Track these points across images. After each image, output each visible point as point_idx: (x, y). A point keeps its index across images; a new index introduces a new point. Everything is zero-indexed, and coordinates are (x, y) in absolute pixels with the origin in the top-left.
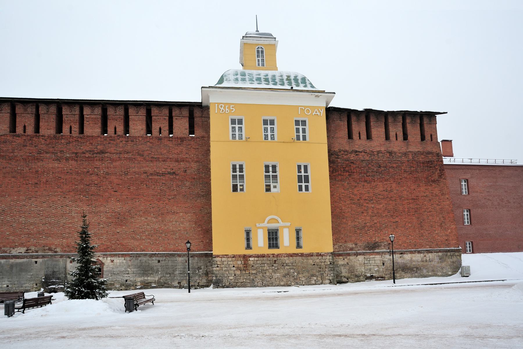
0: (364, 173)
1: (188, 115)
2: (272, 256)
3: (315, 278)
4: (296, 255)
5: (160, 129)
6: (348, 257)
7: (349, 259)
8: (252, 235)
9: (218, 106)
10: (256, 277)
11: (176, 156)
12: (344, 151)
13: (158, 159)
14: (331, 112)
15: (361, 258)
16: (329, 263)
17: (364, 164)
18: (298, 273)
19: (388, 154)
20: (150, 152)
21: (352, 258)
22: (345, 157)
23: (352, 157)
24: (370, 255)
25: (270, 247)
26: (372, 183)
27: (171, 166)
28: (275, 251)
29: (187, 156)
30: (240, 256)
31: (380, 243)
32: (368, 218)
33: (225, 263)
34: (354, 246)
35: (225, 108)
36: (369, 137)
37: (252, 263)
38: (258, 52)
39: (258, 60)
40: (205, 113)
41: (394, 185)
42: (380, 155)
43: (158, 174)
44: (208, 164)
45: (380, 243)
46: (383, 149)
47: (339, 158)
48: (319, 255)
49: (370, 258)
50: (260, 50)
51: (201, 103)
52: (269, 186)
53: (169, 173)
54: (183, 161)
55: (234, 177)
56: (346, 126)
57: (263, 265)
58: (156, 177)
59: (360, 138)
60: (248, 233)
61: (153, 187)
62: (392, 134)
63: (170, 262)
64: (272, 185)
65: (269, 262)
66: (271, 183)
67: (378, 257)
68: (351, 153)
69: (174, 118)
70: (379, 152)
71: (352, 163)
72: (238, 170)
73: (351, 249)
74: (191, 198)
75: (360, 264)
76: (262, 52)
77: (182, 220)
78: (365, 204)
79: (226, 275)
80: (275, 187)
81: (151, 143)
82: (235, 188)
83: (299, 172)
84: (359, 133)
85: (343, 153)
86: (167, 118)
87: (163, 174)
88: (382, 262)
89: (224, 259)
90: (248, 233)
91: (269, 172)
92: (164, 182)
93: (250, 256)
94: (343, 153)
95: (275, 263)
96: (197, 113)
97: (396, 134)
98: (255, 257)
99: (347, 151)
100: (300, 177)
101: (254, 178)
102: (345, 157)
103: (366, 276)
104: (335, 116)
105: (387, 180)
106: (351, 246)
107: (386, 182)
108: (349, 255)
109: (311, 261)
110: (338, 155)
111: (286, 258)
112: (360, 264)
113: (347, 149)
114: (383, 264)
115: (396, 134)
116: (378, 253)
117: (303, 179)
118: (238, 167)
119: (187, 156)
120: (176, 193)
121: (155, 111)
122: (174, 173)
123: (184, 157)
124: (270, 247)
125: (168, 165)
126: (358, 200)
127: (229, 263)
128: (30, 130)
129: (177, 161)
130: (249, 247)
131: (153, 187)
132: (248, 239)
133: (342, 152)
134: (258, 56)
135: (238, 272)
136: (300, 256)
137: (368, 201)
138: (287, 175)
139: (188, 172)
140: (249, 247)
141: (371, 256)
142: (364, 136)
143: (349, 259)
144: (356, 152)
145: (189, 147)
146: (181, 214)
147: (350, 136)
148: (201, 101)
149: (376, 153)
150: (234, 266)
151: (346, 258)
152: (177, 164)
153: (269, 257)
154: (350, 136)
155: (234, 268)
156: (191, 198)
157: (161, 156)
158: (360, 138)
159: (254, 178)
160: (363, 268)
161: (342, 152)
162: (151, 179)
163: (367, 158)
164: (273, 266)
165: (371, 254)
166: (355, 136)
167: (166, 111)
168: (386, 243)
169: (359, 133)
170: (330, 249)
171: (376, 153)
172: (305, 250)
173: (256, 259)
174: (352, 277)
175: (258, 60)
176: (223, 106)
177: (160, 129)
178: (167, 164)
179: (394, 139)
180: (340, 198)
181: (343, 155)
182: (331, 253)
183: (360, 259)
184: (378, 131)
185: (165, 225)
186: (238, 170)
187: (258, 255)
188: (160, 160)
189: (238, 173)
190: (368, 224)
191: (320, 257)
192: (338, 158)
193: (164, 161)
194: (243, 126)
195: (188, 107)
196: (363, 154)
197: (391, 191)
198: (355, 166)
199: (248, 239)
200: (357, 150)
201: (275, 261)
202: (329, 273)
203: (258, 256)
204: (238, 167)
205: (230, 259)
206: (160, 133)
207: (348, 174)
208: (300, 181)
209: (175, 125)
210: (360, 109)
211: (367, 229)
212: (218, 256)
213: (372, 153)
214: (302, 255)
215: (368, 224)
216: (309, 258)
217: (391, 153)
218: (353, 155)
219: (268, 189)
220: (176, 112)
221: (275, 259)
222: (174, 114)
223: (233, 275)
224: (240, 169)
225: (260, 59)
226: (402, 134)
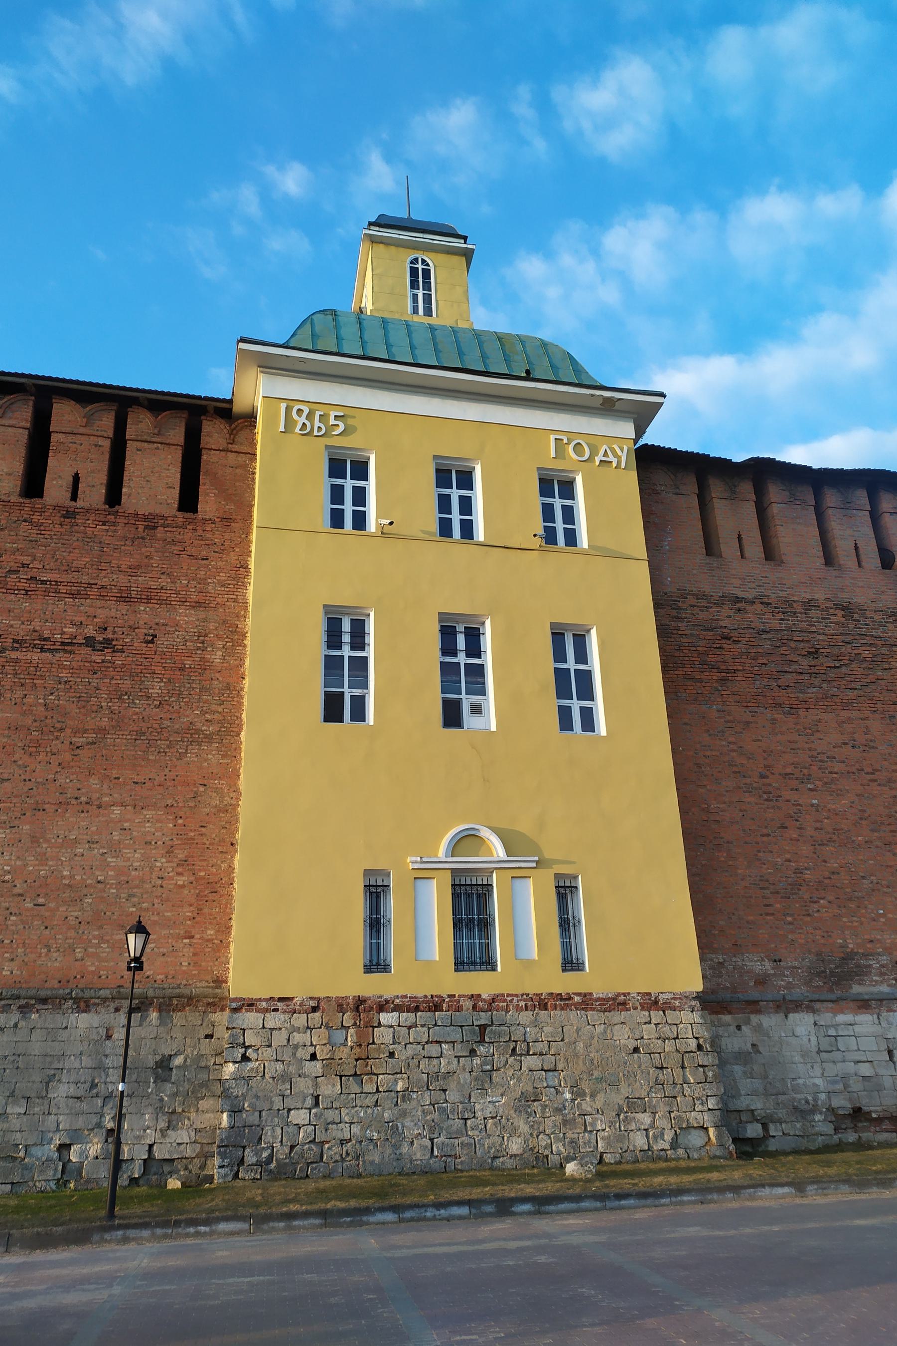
0: (770, 677)
1: (181, 441)
2: (468, 1004)
3: (645, 1119)
4: (563, 1001)
5: (76, 478)
6: (755, 1019)
7: (760, 1025)
8: (392, 906)
9: (288, 409)
10: (404, 1114)
11: (123, 580)
12: (697, 596)
13: (51, 588)
14: (651, 460)
15: (802, 1024)
16: (693, 1044)
17: (767, 646)
18: (578, 1094)
19: (840, 613)
20: (26, 560)
21: (769, 1021)
22: (702, 616)
23: (726, 617)
24: (836, 1013)
25: (460, 965)
26: (802, 712)
27: (102, 614)
28: (481, 983)
29: (164, 581)
30: (341, 1006)
31: (865, 956)
32: (805, 849)
33: (279, 1039)
34: (768, 965)
35: (310, 416)
36: (770, 554)
37: (389, 1039)
38: (414, 272)
39: (415, 298)
40: (242, 436)
41: (876, 725)
42: (813, 613)
43: (43, 644)
44: (238, 616)
45: (865, 956)
46: (820, 596)
47: (681, 619)
48: (651, 1003)
49: (836, 1026)
50: (420, 266)
51: (230, 402)
52: (457, 704)
53: (90, 642)
54: (149, 600)
55: (332, 665)
56: (697, 514)
57: (434, 1050)
58: (36, 656)
59: (742, 556)
60: (375, 893)
61: (19, 693)
62: (843, 547)
63: (37, 1035)
64: (467, 701)
65: (458, 1037)
66: (463, 696)
67: (865, 1022)
68: (720, 603)
69: (131, 447)
70: (809, 605)
71: (727, 638)
72: (346, 638)
73: (762, 981)
74: (163, 744)
75: (805, 1054)
76: (426, 273)
77: (116, 836)
78: (787, 794)
79: (278, 1103)
80: (476, 710)
81: (38, 525)
82: (333, 710)
83: (559, 654)
84: (740, 538)
85: (693, 601)
86: (107, 444)
87: (67, 646)
88: (884, 1047)
89: (273, 1021)
90: (375, 893)
91: (339, 647)
92: (64, 674)
93: (383, 1006)
94: (693, 601)
95: (482, 1041)
96: (213, 433)
97: (856, 548)
98: (398, 1009)
99: (703, 596)
100: (561, 676)
101: (399, 669)
102: (702, 616)
103: (832, 1110)
104: (662, 478)
105: (846, 706)
106: (758, 967)
107: (846, 714)
108: (754, 1006)
109: (623, 1037)
110: (679, 608)
111: (525, 1017)
112: (805, 1054)
113: (707, 588)
114: (890, 1053)
115: (856, 548)
116: (864, 1004)
117: (572, 685)
118: (346, 626)
119: (164, 581)
120: (105, 722)
121: (64, 415)
122: (107, 643)
123: (153, 584)
124: (460, 965)
125: (91, 611)
126: (763, 777)
127: (297, 1038)
128: (94, 493)
129: (125, 598)
130: (376, 964)
131: (19, 693)
132: (375, 924)
133: (691, 600)
134: (414, 285)
135: (329, 1089)
136: (579, 1007)
137: (795, 783)
138: (512, 667)
139: (162, 641)
140: (376, 964)
141: (841, 1018)
142: (754, 548)
143: (759, 1028)
144: (738, 600)
145: (176, 549)
146: (117, 810)
147: (710, 547)
148: (229, 397)
149: (799, 608)
150: (313, 1057)
151: (748, 1022)
152: (124, 608)
153: (459, 1009)
154: (710, 547)
155: (316, 1068)
156: (163, 744)
157: (65, 578)
158: (742, 556)
159: (399, 669)
160: (818, 1071)
161: (691, 600)
162: (17, 661)
163: (775, 624)
164: (473, 1053)
165: (839, 1003)
166: (728, 547)
167: (106, 422)
168: (884, 959)
169: (740, 538)
170: (698, 986)
171: (799, 608)
172: (592, 980)
173: (407, 1018)
174: (782, 1113)
175: (415, 298)
176: (306, 411)
177: (76, 478)
178: (86, 606)
179: (852, 563)
180: (699, 766)
181: (696, 610)
182: (698, 997)
183: (801, 1030)
184: (795, 530)
185: (43, 859)
186: (346, 638)
187: (413, 999)
188: (63, 589)
189: (346, 652)
190: (808, 875)
191: (657, 1016)
192: (679, 619)
193: (74, 595)
194: (371, 486)
195: (185, 415)
196: (759, 607)
197: (869, 746)
198: (736, 648)
199: (375, 924)
200: (741, 594)
201: (483, 1028)
202: (698, 1091)
203: (413, 1006)
204: (346, 626)
205: (300, 1020)
206: (74, 497)
207: (715, 675)
208: (563, 691)
209: (131, 469)
210: (739, 457)
211: (807, 896)
212: (251, 1005)
213: (786, 608)
214: (587, 1002)
215: (808, 875)
216: (617, 1016)
217: (847, 609)
218: (726, 611)
219: (452, 716)
220: (140, 424)
221: (484, 1018)
222: (130, 433)
223: (309, 1102)
224: (353, 634)
225: (420, 293)
226: (102, 477)
